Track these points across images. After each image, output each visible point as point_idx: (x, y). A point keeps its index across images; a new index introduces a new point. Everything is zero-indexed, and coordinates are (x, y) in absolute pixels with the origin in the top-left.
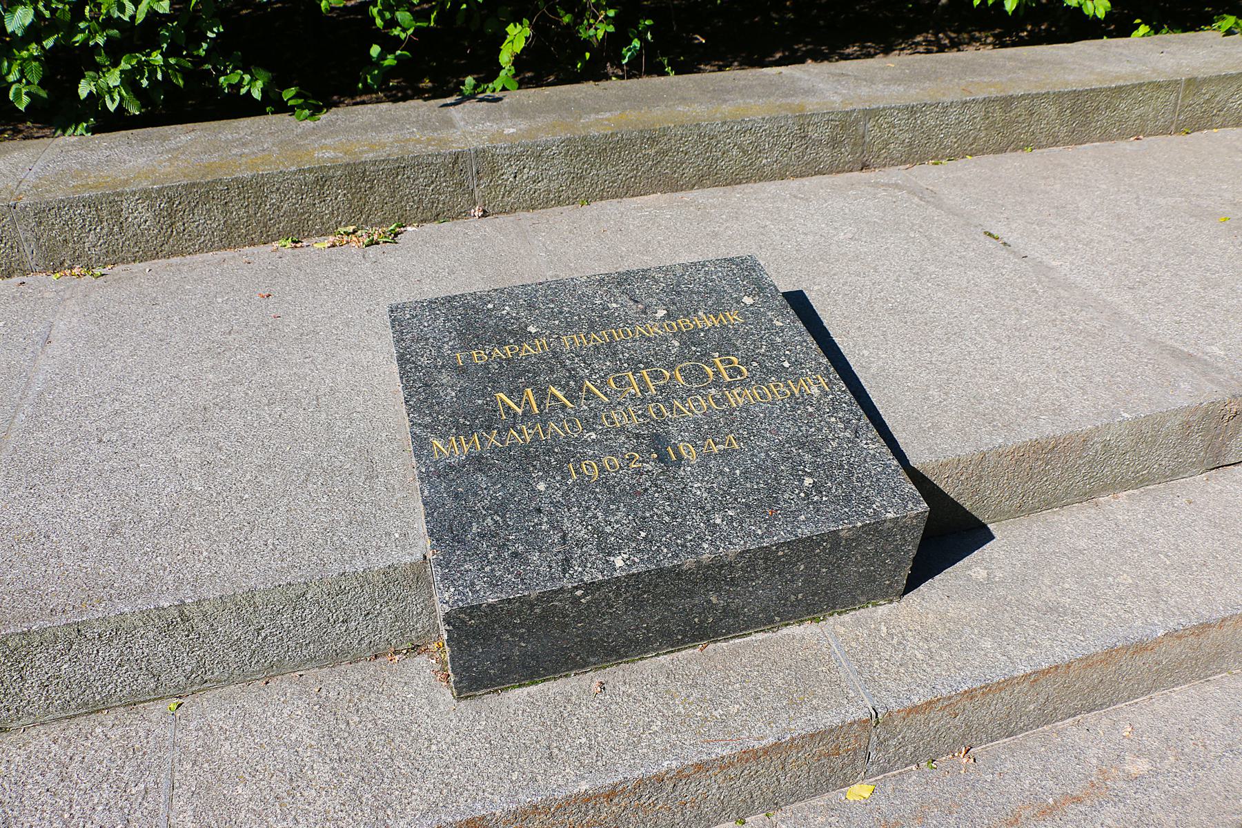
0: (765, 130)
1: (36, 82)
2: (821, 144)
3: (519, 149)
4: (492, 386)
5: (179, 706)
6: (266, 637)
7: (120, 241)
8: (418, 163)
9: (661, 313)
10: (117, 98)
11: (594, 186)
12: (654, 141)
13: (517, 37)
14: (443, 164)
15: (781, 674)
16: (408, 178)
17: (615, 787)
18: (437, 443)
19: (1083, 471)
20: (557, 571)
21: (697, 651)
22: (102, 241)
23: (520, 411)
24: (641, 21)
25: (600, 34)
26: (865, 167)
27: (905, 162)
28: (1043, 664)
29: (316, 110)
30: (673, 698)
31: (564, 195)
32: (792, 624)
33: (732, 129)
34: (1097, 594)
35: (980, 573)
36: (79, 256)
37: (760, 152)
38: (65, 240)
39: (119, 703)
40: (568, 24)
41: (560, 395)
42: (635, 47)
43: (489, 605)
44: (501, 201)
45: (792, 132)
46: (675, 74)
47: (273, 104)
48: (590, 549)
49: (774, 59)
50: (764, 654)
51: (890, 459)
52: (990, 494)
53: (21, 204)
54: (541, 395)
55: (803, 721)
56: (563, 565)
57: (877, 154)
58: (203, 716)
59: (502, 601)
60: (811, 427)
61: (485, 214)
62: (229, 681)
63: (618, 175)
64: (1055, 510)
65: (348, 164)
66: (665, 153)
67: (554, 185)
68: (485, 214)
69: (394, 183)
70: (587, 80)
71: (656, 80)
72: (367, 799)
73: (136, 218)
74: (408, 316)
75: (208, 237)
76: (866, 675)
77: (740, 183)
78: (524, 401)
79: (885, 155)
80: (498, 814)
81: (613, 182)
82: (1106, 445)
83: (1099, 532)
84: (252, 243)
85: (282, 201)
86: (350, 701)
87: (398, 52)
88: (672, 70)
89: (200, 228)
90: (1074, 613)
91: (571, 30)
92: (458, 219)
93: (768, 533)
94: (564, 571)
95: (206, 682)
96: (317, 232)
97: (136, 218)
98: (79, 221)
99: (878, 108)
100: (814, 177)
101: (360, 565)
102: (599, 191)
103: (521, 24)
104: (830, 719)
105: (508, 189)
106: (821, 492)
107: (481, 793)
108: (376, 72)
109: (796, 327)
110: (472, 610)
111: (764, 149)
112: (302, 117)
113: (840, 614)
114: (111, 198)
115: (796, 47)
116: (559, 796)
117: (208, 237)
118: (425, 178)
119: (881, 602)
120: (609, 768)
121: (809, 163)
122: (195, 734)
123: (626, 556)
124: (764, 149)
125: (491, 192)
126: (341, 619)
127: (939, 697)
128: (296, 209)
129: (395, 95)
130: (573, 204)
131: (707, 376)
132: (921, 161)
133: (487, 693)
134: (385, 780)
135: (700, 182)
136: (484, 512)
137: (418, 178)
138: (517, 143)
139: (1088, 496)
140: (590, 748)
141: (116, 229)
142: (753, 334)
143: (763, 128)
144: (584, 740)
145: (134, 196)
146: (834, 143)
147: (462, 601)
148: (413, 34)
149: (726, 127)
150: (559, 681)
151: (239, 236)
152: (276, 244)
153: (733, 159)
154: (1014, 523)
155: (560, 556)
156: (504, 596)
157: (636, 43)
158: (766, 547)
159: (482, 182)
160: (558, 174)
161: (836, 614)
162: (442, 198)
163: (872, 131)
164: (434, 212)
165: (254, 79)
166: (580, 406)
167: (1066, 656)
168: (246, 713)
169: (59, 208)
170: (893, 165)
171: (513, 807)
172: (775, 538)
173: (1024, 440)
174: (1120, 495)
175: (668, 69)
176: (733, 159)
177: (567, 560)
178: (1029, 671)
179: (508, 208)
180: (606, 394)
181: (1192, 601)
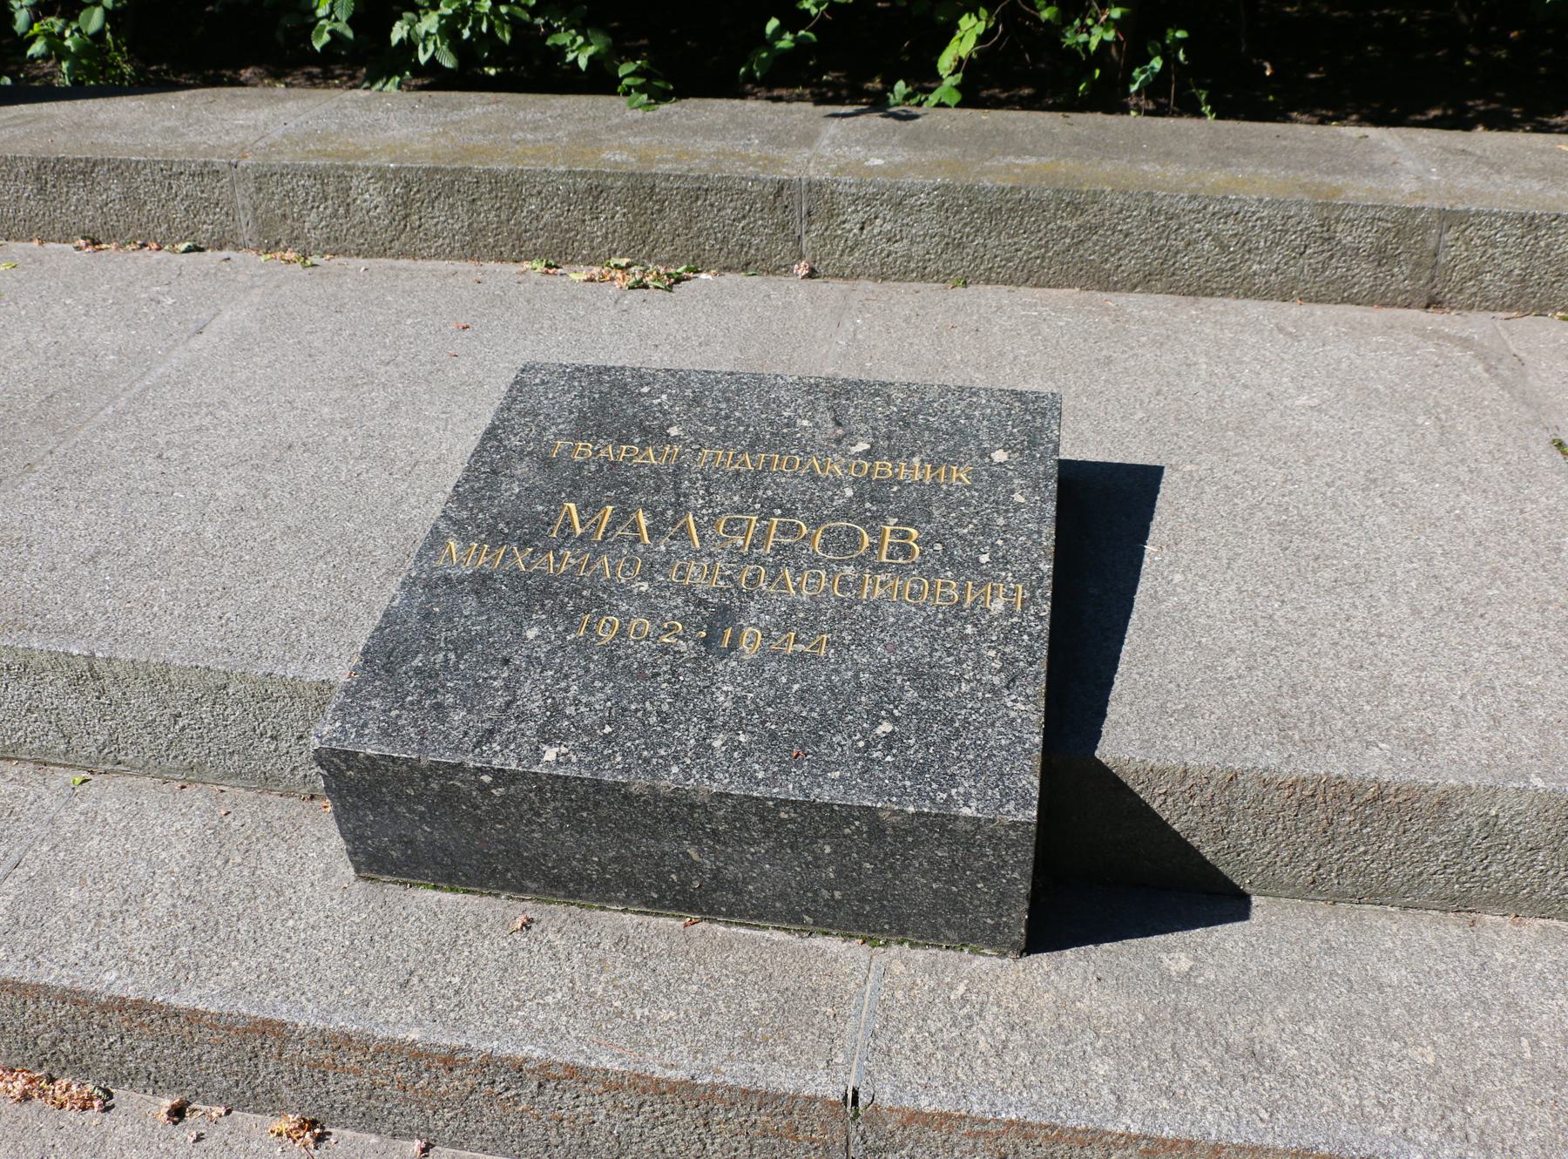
0: (1261, 219)
1: (344, 19)
2: (1357, 254)
3: (871, 190)
4: (571, 492)
5: (85, 781)
6: (183, 729)
7: (345, 227)
8: (727, 188)
9: (863, 446)
10: (431, 48)
11: (978, 261)
12: (1076, 208)
13: (969, 32)
14: (760, 193)
15: (765, 995)
16: (712, 205)
17: (453, 1052)
18: (453, 545)
19: (1442, 857)
20: (468, 743)
21: (680, 924)
22: (323, 223)
23: (579, 531)
24: (217, 10)
25: (1094, 44)
26: (1433, 303)
27: (1510, 307)
28: (1167, 1129)
29: (661, 97)
30: (600, 972)
31: (931, 268)
32: (834, 936)
33: (1205, 208)
34: (1353, 1060)
35: (1180, 962)
36: (297, 238)
37: (1249, 251)
38: (284, 216)
39: (28, 757)
40: (1048, 21)
41: (644, 523)
42: (1153, 68)
43: (368, 757)
44: (839, 260)
45: (1307, 229)
46: (1217, 118)
47: (599, 81)
48: (530, 729)
49: (1424, 118)
50: (765, 961)
51: (1031, 733)
52: (1252, 844)
53: (243, 164)
54: (622, 515)
55: (743, 1066)
56: (482, 736)
57: (1459, 287)
58: (98, 800)
59: (384, 757)
60: (949, 655)
61: (812, 274)
62: (144, 771)
63: (1017, 250)
64: (1389, 908)
65: (633, 174)
66: (1094, 229)
67: (919, 251)
68: (812, 274)
69: (690, 209)
70: (1093, 109)
71: (1186, 123)
72: (182, 952)
73: (365, 201)
74: (537, 381)
75: (447, 241)
76: (882, 1043)
77: (1212, 295)
78: (593, 521)
79: (1474, 289)
80: (301, 1027)
81: (1009, 260)
82: (1489, 824)
83: (1441, 967)
84: (500, 258)
85: (542, 210)
86: (247, 838)
87: (802, 32)
88: (1212, 112)
89: (439, 227)
90: (1288, 1076)
91: (1053, 32)
92: (774, 274)
93: (771, 781)
94: (478, 744)
95: (119, 763)
96: (584, 259)
97: (365, 201)
98: (301, 193)
99: (1467, 211)
100: (1338, 306)
101: (293, 670)
102: (985, 270)
103: (977, 16)
104: (783, 1080)
105: (849, 243)
106: (891, 748)
107: (298, 994)
108: (764, 55)
109: (1041, 509)
110: (350, 757)
111: (1257, 248)
112: (635, 104)
113: (913, 945)
114: (340, 172)
115: (1470, 103)
116: (382, 1033)
117: (447, 241)
118: (735, 209)
119: (986, 951)
120: (458, 1026)
121: (1333, 282)
122: (77, 816)
123: (564, 750)
124: (1257, 248)
125: (825, 245)
126: (269, 734)
127: (963, 1112)
128: (560, 223)
129: (825, 94)
130: (944, 282)
131: (857, 546)
132: (1541, 311)
133: (394, 883)
134: (215, 939)
135: (1145, 281)
136: (442, 645)
137: (724, 208)
138: (869, 180)
139: (1461, 904)
140: (457, 992)
141: (341, 211)
142: (969, 505)
143: (1258, 215)
144: (457, 980)
145: (367, 172)
146: (1381, 256)
147: (338, 740)
148: (826, 10)
149: (1195, 205)
150: (485, 899)
151: (485, 246)
152: (526, 265)
153: (1203, 256)
154: (1299, 907)
155: (487, 725)
156: (387, 751)
157: (1157, 63)
158: (757, 798)
159: (813, 227)
160: (925, 235)
161: (906, 945)
162: (755, 241)
163: (1453, 247)
164: (743, 259)
165: (587, 43)
166: (657, 545)
167: (1214, 1132)
168: (139, 814)
169: (282, 175)
170: (1486, 308)
171: (320, 1025)
172: (775, 790)
173: (1316, 770)
174: (1527, 921)
175: (1206, 109)
176: (1203, 256)
177: (491, 732)
178: (1134, 1130)
179: (847, 272)
180: (701, 538)
181: (1520, 1131)
